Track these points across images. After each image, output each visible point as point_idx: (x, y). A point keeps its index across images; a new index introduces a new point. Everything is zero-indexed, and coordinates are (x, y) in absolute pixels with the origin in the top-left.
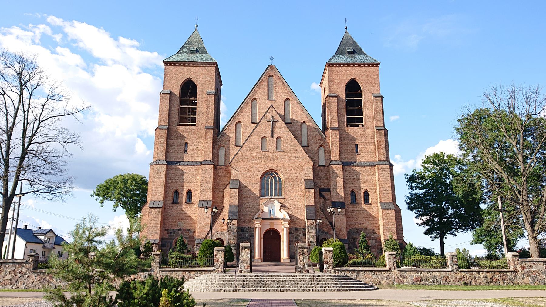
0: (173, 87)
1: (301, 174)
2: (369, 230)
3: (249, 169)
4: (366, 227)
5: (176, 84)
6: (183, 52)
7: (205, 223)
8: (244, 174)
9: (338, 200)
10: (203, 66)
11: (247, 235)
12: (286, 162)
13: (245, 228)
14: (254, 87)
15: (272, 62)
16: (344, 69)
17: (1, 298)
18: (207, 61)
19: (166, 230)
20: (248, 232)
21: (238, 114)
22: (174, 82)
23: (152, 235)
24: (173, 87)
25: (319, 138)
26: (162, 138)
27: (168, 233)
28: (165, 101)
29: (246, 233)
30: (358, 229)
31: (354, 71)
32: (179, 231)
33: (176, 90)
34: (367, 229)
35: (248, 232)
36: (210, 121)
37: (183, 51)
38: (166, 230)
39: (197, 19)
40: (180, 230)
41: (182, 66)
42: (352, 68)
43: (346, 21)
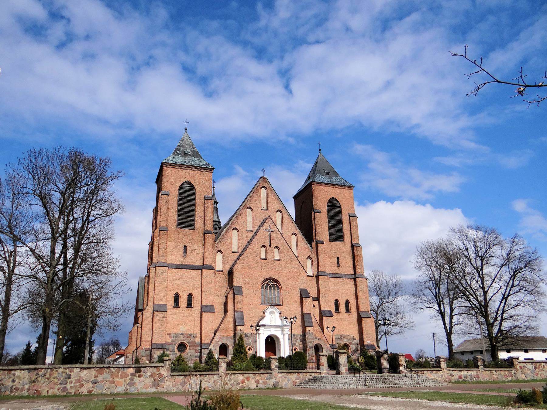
0: (171, 188)
1: (296, 283)
2: (350, 336)
3: (250, 275)
4: (348, 334)
5: (174, 186)
6: (178, 154)
7: (210, 328)
8: (246, 281)
9: (326, 309)
10: (200, 171)
11: (250, 341)
12: (283, 271)
13: (248, 333)
14: (248, 195)
15: (264, 174)
16: (326, 188)
17: (546, 362)
18: (205, 167)
19: (168, 334)
20: (252, 338)
21: (234, 220)
22: (173, 184)
23: (158, 339)
24: (171, 188)
25: (307, 250)
26: (163, 240)
27: (170, 337)
28: (165, 202)
29: (250, 338)
30: (341, 336)
31: (334, 191)
32: (182, 336)
33: (174, 192)
34: (348, 335)
35: (252, 338)
36: (208, 225)
37: (178, 153)
38: (168, 334)
39: (186, 122)
40: (182, 334)
41: (180, 169)
42: (333, 188)
43: (319, 144)
